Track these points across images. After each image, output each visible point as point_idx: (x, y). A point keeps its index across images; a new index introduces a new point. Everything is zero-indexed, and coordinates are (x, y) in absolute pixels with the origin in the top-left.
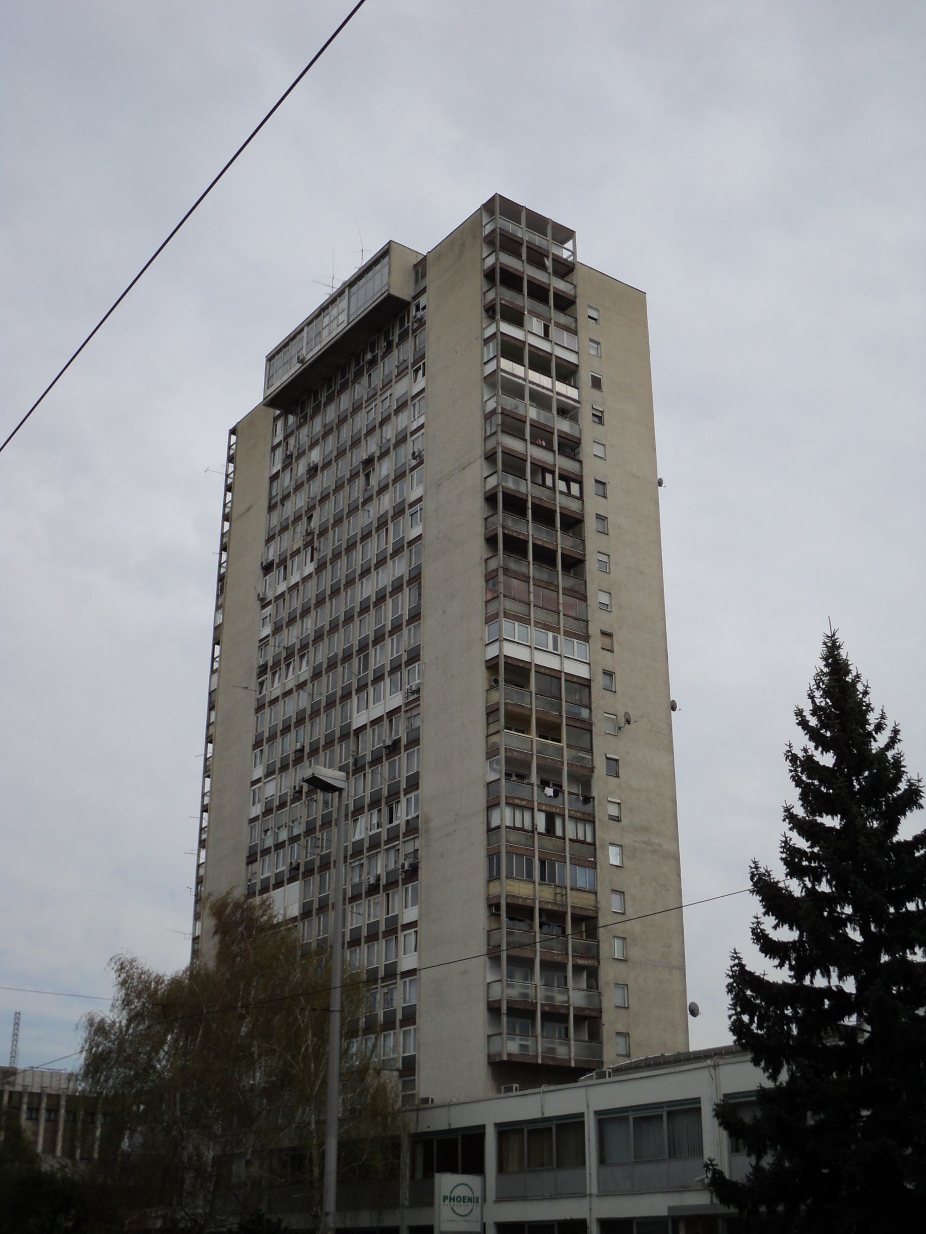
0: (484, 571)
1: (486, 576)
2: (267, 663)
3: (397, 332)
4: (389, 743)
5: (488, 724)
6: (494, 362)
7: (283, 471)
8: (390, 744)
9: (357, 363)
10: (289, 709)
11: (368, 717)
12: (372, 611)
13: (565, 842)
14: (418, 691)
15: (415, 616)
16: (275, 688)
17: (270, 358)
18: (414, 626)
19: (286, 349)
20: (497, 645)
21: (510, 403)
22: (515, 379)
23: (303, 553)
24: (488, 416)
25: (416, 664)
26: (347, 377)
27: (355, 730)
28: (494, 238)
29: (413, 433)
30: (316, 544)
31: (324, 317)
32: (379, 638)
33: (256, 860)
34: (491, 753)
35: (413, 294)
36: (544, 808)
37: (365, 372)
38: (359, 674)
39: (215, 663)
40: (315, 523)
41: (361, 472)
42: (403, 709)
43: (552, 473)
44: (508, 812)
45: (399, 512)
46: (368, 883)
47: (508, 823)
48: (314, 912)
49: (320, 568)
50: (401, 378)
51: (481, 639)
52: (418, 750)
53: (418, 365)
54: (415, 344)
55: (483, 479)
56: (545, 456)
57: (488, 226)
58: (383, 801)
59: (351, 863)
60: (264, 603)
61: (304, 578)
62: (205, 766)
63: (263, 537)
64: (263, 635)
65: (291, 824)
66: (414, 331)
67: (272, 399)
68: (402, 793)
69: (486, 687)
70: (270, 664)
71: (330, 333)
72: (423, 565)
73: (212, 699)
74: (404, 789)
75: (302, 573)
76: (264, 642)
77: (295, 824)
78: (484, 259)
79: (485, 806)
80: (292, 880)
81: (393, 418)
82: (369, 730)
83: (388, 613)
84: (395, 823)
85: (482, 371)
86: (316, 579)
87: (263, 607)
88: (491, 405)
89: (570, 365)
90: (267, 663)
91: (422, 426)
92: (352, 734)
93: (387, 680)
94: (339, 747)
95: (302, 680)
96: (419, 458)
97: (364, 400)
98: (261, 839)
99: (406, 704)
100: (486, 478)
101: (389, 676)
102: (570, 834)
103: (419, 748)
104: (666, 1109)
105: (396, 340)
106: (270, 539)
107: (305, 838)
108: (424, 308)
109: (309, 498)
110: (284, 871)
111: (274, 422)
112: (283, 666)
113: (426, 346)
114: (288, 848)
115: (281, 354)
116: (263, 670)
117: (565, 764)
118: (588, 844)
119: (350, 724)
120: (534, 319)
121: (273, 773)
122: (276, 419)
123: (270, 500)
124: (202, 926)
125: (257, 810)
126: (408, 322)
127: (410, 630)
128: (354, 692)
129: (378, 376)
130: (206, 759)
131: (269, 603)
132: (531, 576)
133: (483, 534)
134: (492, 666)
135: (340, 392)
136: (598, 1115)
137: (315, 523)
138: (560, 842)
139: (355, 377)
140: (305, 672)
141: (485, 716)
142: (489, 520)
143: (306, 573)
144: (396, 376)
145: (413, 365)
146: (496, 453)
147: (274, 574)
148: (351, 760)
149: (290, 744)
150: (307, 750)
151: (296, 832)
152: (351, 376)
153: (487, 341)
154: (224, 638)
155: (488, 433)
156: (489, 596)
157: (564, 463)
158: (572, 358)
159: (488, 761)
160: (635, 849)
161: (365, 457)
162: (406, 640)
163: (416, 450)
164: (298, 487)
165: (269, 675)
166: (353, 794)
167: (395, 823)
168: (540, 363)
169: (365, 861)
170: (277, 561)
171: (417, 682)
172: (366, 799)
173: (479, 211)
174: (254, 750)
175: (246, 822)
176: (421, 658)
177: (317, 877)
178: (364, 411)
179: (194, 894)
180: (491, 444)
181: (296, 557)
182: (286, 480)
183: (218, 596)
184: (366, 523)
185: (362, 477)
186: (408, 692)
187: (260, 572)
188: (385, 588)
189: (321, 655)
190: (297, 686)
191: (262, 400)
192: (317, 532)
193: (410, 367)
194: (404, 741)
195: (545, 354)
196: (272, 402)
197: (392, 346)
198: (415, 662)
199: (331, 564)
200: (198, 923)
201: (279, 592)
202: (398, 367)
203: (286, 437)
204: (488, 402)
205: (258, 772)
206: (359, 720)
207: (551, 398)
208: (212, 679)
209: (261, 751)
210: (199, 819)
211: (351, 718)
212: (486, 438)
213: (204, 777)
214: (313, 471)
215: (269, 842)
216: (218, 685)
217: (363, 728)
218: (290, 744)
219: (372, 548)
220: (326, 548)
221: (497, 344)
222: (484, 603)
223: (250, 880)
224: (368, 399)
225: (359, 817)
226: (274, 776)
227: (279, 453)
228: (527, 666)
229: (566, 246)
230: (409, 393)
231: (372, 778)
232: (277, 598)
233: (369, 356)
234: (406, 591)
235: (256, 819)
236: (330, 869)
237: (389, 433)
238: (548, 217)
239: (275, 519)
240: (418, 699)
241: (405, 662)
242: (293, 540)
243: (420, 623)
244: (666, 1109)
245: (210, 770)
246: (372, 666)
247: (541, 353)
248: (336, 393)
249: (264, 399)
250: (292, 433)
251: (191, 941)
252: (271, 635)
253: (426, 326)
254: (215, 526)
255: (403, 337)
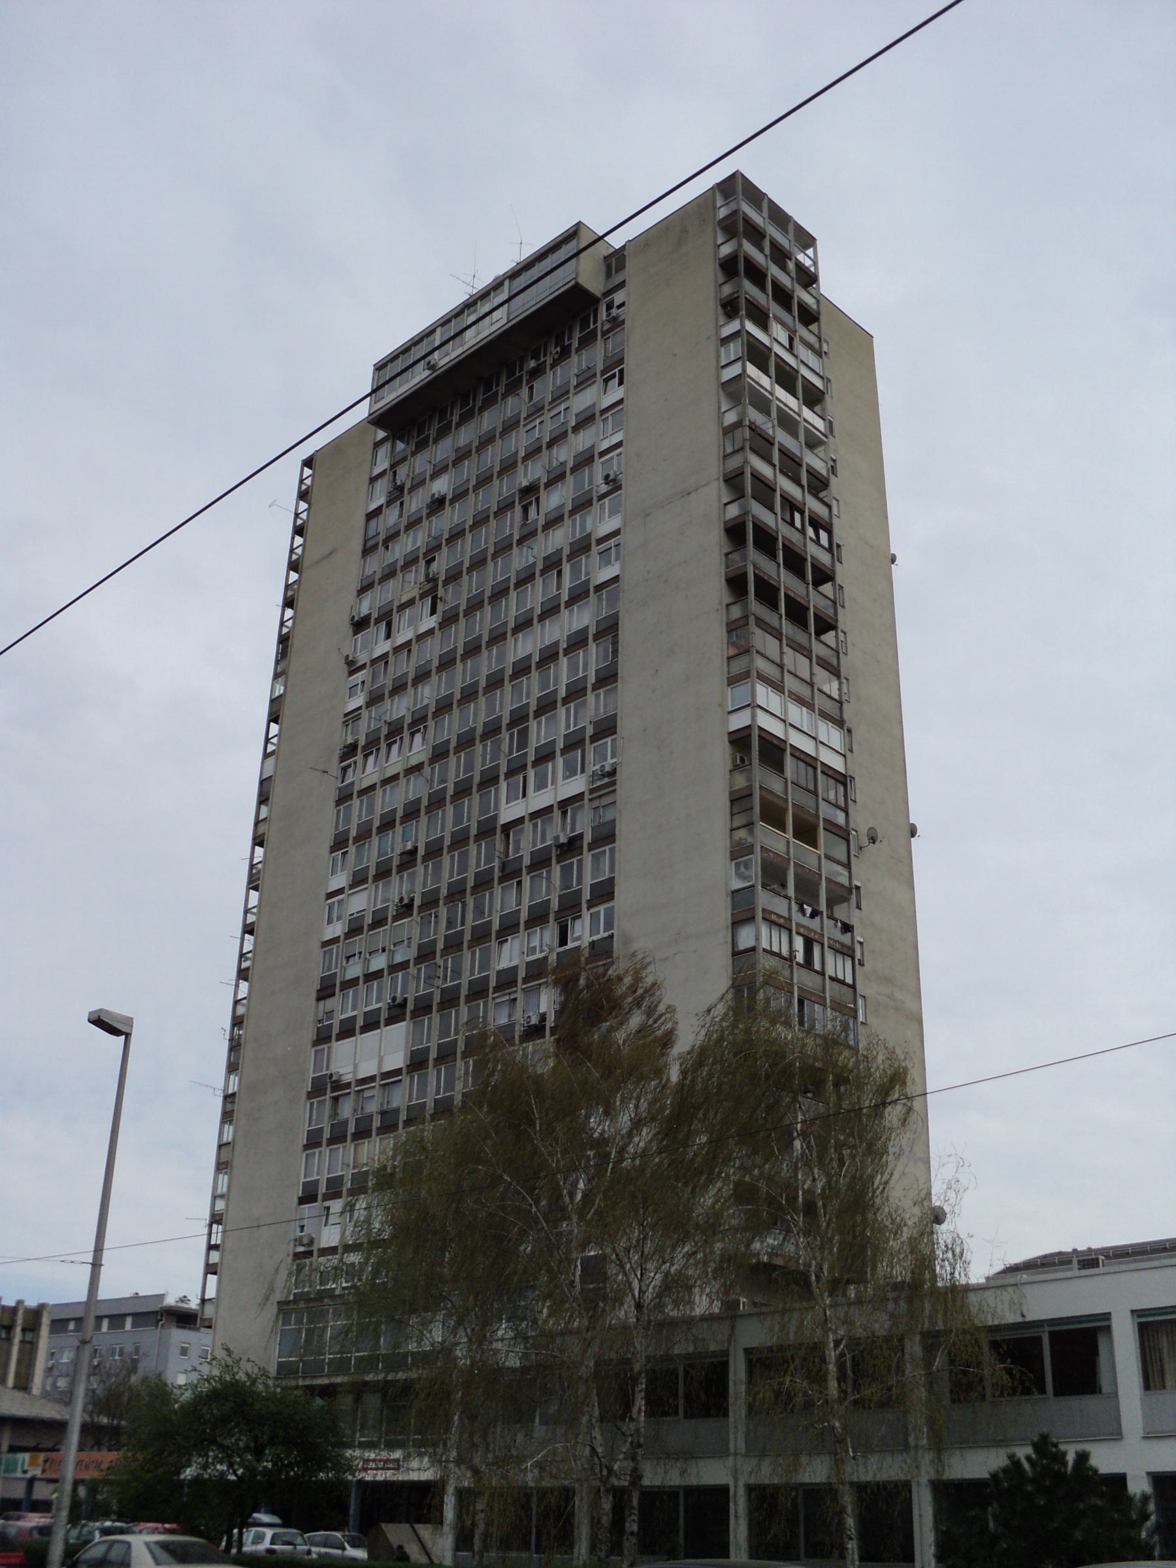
0: (725, 619)
1: (728, 625)
2: (356, 741)
3: (577, 335)
4: (563, 839)
5: (732, 815)
6: (738, 365)
7: (387, 507)
8: (566, 841)
9: (511, 373)
10: (394, 799)
11: (527, 807)
12: (535, 674)
13: (824, 979)
14: (613, 773)
15: (608, 678)
16: (370, 771)
17: (380, 367)
18: (605, 692)
19: (393, 364)
20: (748, 712)
21: (754, 415)
22: (762, 390)
23: (418, 603)
24: (728, 431)
25: (609, 740)
26: (494, 390)
27: (503, 825)
28: (736, 221)
29: (603, 454)
30: (441, 592)
31: (468, 315)
32: (546, 706)
33: (333, 995)
34: (739, 852)
35: (603, 291)
36: (802, 930)
37: (524, 383)
38: (511, 753)
39: (269, 745)
40: (440, 566)
41: (517, 502)
42: (587, 797)
43: (802, 513)
44: (764, 930)
45: (581, 547)
46: (528, 1022)
47: (765, 944)
48: (431, 1063)
49: (449, 620)
50: (582, 390)
51: (720, 705)
52: (612, 850)
53: (615, 370)
54: (605, 349)
55: (722, 506)
56: (794, 491)
57: (722, 210)
58: (552, 917)
59: (494, 999)
60: (353, 667)
61: (397, 647)
62: (251, 875)
63: (355, 586)
64: (351, 707)
65: (392, 948)
66: (604, 333)
67: (382, 415)
68: (584, 906)
69: (729, 766)
70: (362, 742)
71: (478, 334)
72: (621, 615)
73: (264, 789)
74: (588, 901)
75: (416, 629)
76: (352, 717)
77: (397, 948)
78: (719, 246)
79: (730, 921)
80: (390, 1021)
81: (571, 436)
82: (528, 826)
83: (562, 674)
84: (571, 945)
85: (718, 377)
86: (440, 637)
87: (351, 673)
88: (731, 418)
89: (814, 389)
90: (356, 741)
91: (619, 444)
92: (499, 830)
93: (560, 761)
94: (475, 848)
95: (414, 762)
96: (614, 484)
97: (474, 446)
98: (342, 967)
99: (592, 791)
100: (726, 504)
101: (562, 754)
102: (830, 971)
103: (614, 848)
104: (1047, 1329)
105: (575, 344)
106: (364, 589)
107: (415, 965)
108: (619, 307)
109: (429, 536)
110: (380, 1009)
111: (374, 448)
112: (383, 746)
113: (626, 350)
114: (387, 980)
115: (544, 262)
116: (350, 750)
117: (824, 878)
118: (848, 985)
119: (495, 818)
120: (779, 326)
121: (364, 881)
122: (378, 445)
123: (365, 542)
124: (240, 1081)
125: (337, 929)
126: (595, 322)
127: (598, 696)
128: (502, 777)
129: (545, 387)
130: (252, 866)
131: (363, 667)
132: (784, 632)
133: (723, 574)
134: (740, 740)
135: (482, 409)
136: (1139, 1316)
137: (440, 566)
138: (819, 978)
139: (506, 391)
140: (418, 749)
141: (728, 804)
142: (730, 556)
143: (423, 628)
144: (576, 387)
145: (603, 373)
146: (743, 473)
147: (371, 629)
148: (496, 864)
149: (396, 843)
150: (421, 852)
151: (399, 958)
152: (433, 433)
153: (725, 341)
154: (286, 713)
155: (729, 450)
156: (732, 652)
157: (812, 504)
158: (818, 383)
159: (733, 863)
160: (878, 1004)
161: (525, 483)
162: (594, 707)
163: (611, 473)
164: (414, 523)
165: (359, 757)
166: (499, 908)
167: (571, 945)
168: (787, 378)
169: (519, 995)
170: (375, 615)
171: (610, 761)
172: (522, 915)
173: (711, 192)
174: (331, 852)
175: (318, 945)
176: (618, 730)
177: (436, 1017)
178: (547, 416)
179: (228, 1037)
180: (734, 463)
181: (407, 610)
182: (391, 517)
183: (277, 662)
184: (524, 565)
185: (518, 509)
186: (593, 776)
187: (349, 630)
188: (557, 643)
189: (450, 728)
190: (405, 770)
191: (367, 415)
192: (442, 577)
193: (598, 375)
194: (588, 838)
195: (791, 370)
196: (378, 420)
197: (570, 352)
198: (607, 737)
199: (464, 616)
200: (232, 1077)
201: (378, 652)
202: (577, 376)
203: (393, 466)
204: (726, 414)
205: (340, 880)
206: (509, 812)
207: (797, 423)
208: (265, 764)
209: (344, 854)
210: (239, 940)
211: (497, 807)
212: (726, 457)
213: (249, 889)
214: (438, 504)
215: (354, 970)
216: (275, 772)
217: (521, 820)
218: (396, 843)
219: (536, 596)
220: (455, 597)
221: (743, 344)
222: (725, 661)
223: (320, 1021)
224: (529, 416)
225: (509, 938)
226: (366, 886)
227: (383, 486)
228: (782, 746)
229: (807, 252)
230: (597, 407)
231: (531, 886)
232: (374, 662)
233: (532, 364)
234: (592, 647)
235: (335, 940)
236: (458, 1005)
237: (564, 454)
238: (790, 213)
239: (375, 565)
240: (614, 783)
241: (591, 737)
242: (410, 584)
243: (617, 687)
244: (1047, 1329)
245: (258, 879)
246: (534, 742)
247: (787, 368)
248: (476, 410)
249: (370, 415)
250: (404, 459)
251: (221, 1098)
252: (364, 707)
253: (626, 325)
254: (276, 579)
255: (588, 340)
